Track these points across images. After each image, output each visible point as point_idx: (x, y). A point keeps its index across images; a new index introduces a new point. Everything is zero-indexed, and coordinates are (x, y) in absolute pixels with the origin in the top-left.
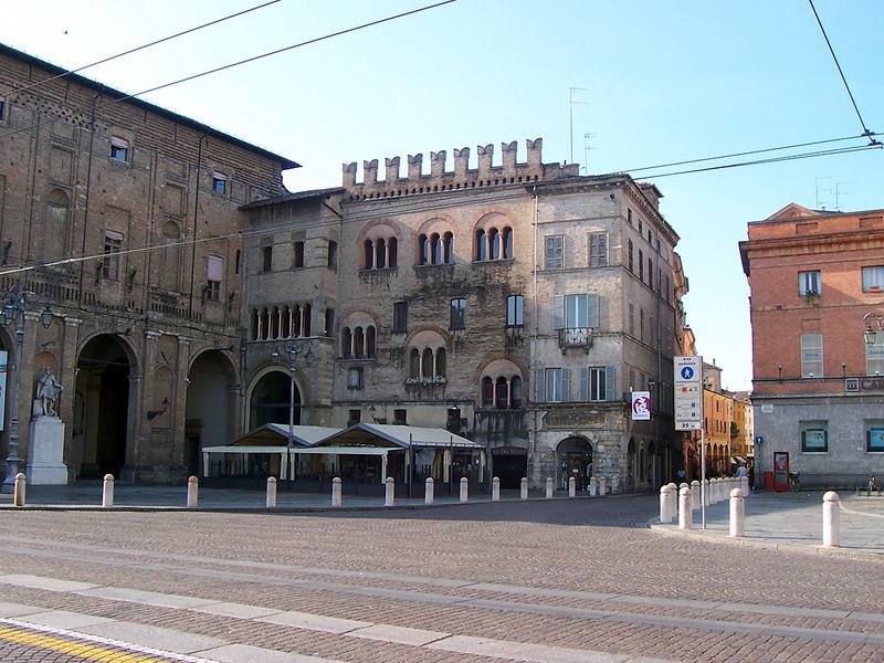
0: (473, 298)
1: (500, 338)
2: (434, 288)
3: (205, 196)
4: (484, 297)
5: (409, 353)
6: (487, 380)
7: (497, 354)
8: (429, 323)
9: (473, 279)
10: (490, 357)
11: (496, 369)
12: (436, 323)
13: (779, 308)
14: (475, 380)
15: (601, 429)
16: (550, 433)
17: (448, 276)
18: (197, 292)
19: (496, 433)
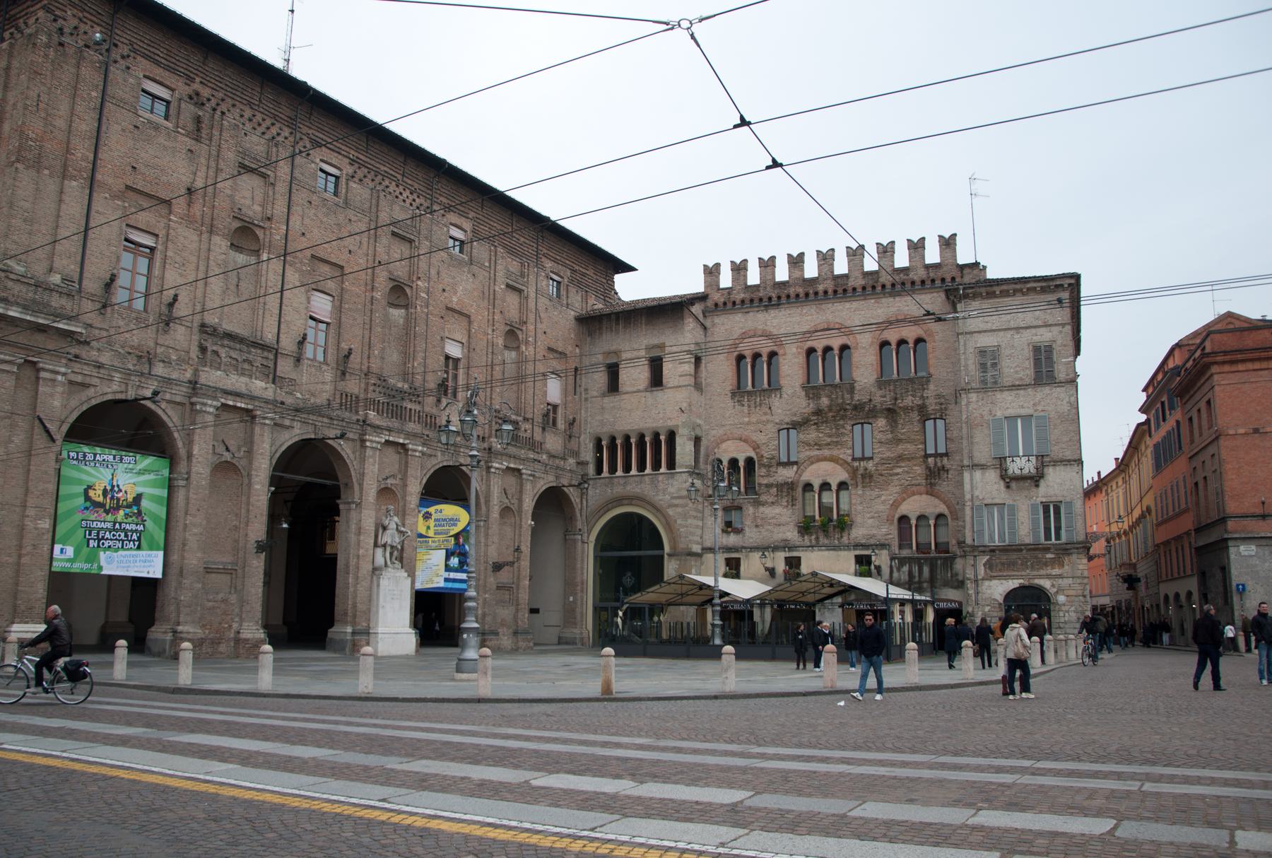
0: (881, 422)
1: (919, 470)
2: (830, 410)
3: (543, 302)
4: (896, 422)
5: (800, 489)
6: (904, 519)
7: (914, 488)
8: (826, 452)
9: (881, 398)
10: (907, 492)
11: (914, 506)
12: (835, 452)
13: (1256, 431)
14: (889, 520)
15: (1060, 576)
16: (995, 582)
17: (847, 396)
18: (538, 419)
19: (920, 582)
